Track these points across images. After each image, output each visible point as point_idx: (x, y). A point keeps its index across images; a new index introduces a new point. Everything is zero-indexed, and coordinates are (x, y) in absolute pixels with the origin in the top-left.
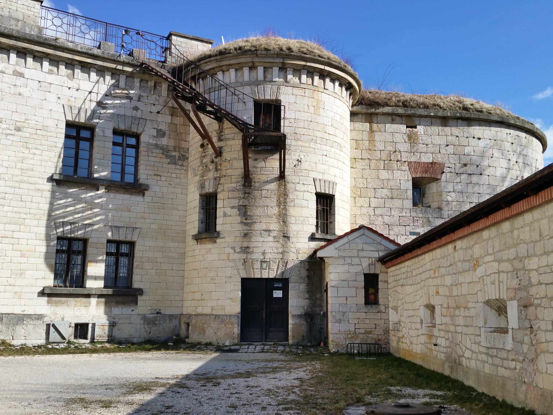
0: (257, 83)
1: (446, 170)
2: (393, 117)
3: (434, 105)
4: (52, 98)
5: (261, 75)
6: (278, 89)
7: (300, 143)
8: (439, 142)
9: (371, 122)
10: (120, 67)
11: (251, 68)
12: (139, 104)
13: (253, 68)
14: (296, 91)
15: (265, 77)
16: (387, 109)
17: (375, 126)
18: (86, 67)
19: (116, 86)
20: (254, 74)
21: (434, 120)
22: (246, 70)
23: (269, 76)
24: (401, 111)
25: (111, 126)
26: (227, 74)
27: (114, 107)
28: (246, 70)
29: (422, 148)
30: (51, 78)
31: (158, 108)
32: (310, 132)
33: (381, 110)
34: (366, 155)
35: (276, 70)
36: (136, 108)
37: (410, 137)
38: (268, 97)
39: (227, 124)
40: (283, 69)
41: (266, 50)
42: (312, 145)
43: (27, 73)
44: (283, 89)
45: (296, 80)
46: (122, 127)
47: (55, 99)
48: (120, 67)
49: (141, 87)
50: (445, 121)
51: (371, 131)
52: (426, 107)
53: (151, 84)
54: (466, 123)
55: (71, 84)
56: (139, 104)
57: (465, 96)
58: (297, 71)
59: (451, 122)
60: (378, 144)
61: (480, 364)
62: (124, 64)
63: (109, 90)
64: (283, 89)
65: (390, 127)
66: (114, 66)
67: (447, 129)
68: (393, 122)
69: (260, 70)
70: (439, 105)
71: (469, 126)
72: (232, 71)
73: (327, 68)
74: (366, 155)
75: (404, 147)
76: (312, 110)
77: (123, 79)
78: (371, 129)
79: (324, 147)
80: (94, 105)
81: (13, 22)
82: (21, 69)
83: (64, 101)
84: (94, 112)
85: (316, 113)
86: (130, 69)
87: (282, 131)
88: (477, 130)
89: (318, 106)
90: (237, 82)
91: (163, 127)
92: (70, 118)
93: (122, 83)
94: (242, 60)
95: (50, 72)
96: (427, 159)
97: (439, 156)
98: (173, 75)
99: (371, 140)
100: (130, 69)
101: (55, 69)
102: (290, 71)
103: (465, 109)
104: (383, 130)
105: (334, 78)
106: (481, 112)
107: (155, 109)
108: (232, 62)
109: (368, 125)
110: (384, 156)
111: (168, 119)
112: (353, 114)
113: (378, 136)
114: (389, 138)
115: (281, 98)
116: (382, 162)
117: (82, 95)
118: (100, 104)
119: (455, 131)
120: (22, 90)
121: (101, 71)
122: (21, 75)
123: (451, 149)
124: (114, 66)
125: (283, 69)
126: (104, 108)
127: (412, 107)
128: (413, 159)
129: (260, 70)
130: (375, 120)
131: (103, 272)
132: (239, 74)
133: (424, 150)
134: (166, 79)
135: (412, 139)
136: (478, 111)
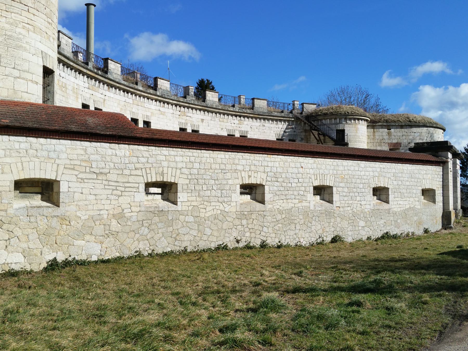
0: (337, 124)
1: (402, 145)
2: (382, 127)
3: (398, 121)
4: (272, 132)
5: (338, 121)
6: (344, 125)
7: (352, 143)
8: (399, 135)
9: (374, 129)
10: (290, 119)
11: (335, 119)
12: (295, 130)
13: (335, 119)
14: (350, 126)
15: (340, 122)
16: (380, 124)
17: (375, 130)
18: (281, 121)
19: (288, 125)
20: (336, 121)
21: (398, 126)
22: (333, 120)
23: (341, 121)
24: (385, 124)
25: (288, 138)
26: (326, 120)
27: (288, 132)
28: (333, 120)
29: (393, 137)
30: (272, 126)
31: (301, 130)
32: (355, 139)
33: (378, 124)
34: (372, 141)
35: (343, 119)
36: (295, 132)
37: (388, 133)
38: (341, 129)
39: (327, 137)
40: (346, 119)
41: (340, 114)
42: (355, 143)
43: (266, 125)
44: (346, 125)
45: (350, 122)
46: (291, 138)
47: (273, 132)
48: (290, 119)
49: (296, 124)
50: (402, 127)
51: (374, 132)
52: (395, 122)
53: (299, 123)
54: (410, 127)
55: (277, 126)
56: (295, 130)
57: (408, 153)
58: (350, 119)
59: (404, 127)
60: (376, 137)
61: (381, 278)
62: (291, 118)
63: (287, 127)
64: (346, 125)
65: (381, 130)
66: (289, 119)
67: (403, 130)
68: (382, 128)
69: (338, 120)
70: (400, 121)
71: (411, 128)
72: (328, 120)
73: (360, 117)
74: (372, 141)
75: (386, 137)
76: (355, 131)
77: (291, 122)
78: (374, 131)
79: (359, 144)
80: (283, 132)
81: (261, 109)
82: (264, 124)
83: (275, 133)
84: (283, 134)
85: (357, 132)
86: (293, 119)
87: (346, 141)
88: (414, 130)
89: (357, 130)
90: (330, 123)
91: (303, 137)
92: (277, 138)
93: (290, 124)
94: (332, 117)
95: (271, 124)
96: (395, 141)
97: (399, 140)
98: (306, 119)
99: (374, 135)
100: (293, 119)
101: (272, 122)
102: (348, 119)
103: (410, 121)
104: (378, 131)
105: (362, 119)
106: (416, 122)
107: (300, 131)
108: (329, 117)
109: (372, 130)
110: (379, 141)
111: (304, 134)
112: (368, 126)
113: (376, 134)
114: (380, 134)
115: (345, 129)
116: (378, 143)
117: (279, 130)
118: (285, 132)
119: (406, 130)
120: (265, 131)
121: (285, 121)
122: (264, 126)
123: (404, 137)
124: (289, 119)
125: (346, 119)
126: (286, 133)
127: (389, 122)
128: (390, 142)
129: (338, 120)
130: (375, 128)
131: (58, 105)
132: (331, 120)
133: (394, 138)
134: (303, 121)
135: (389, 134)
136: (415, 122)
